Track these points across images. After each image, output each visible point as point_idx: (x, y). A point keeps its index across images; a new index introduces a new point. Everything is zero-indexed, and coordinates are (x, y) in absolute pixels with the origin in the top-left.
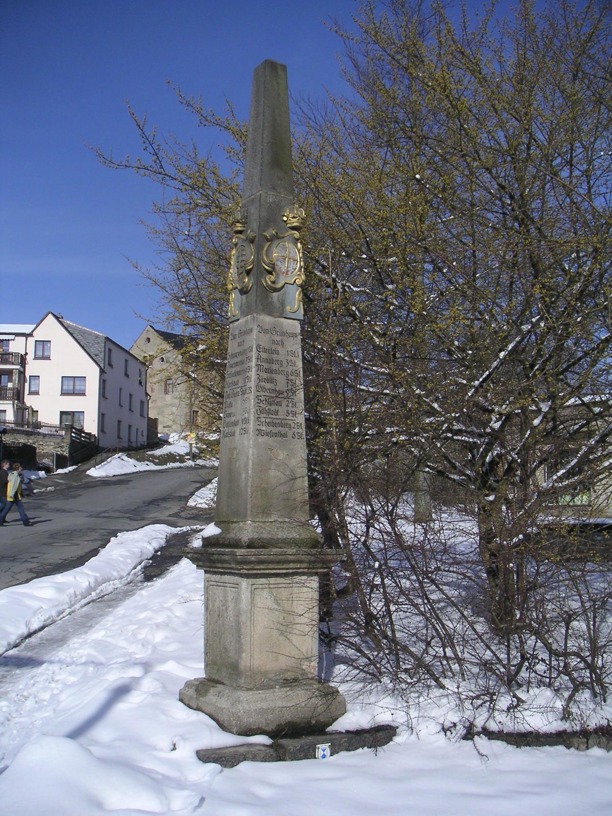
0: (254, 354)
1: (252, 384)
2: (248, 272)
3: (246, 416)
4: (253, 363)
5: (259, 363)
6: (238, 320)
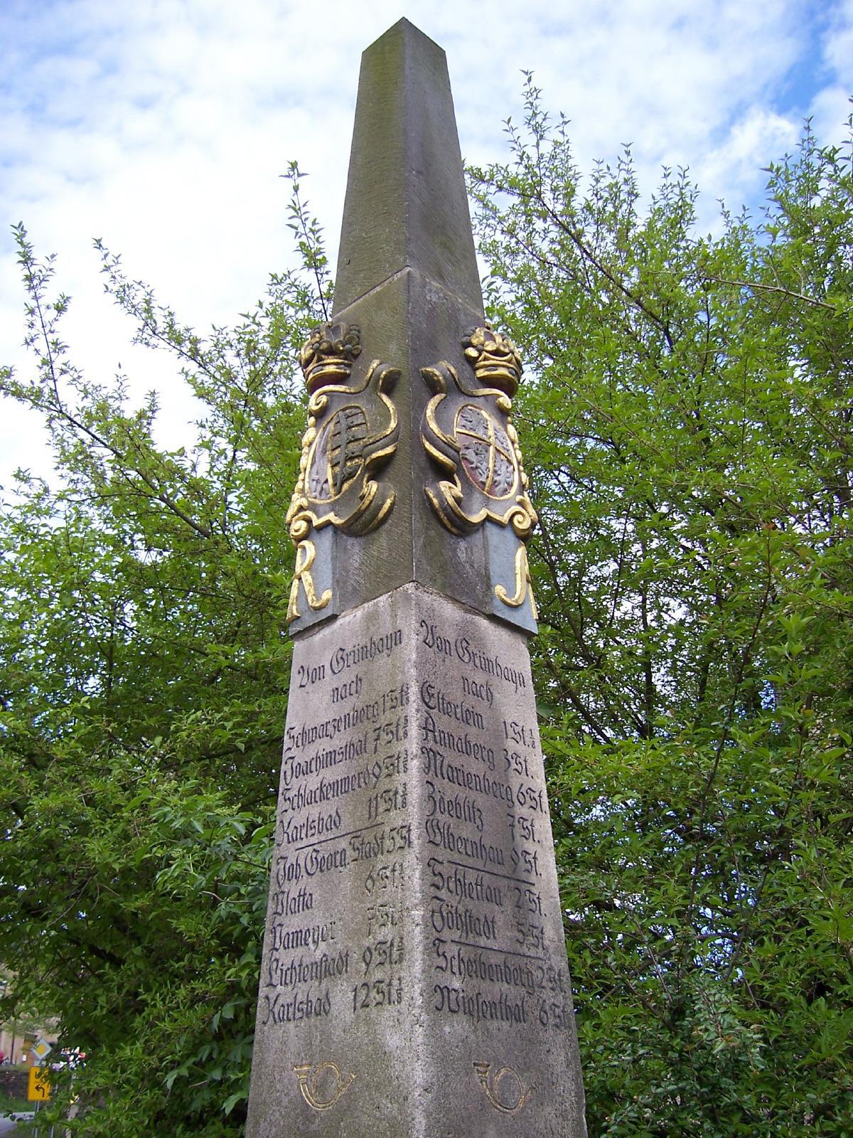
0: (413, 709)
1: (414, 814)
2: (378, 469)
3: (387, 933)
4: (413, 742)
5: (431, 744)
6: (333, 618)
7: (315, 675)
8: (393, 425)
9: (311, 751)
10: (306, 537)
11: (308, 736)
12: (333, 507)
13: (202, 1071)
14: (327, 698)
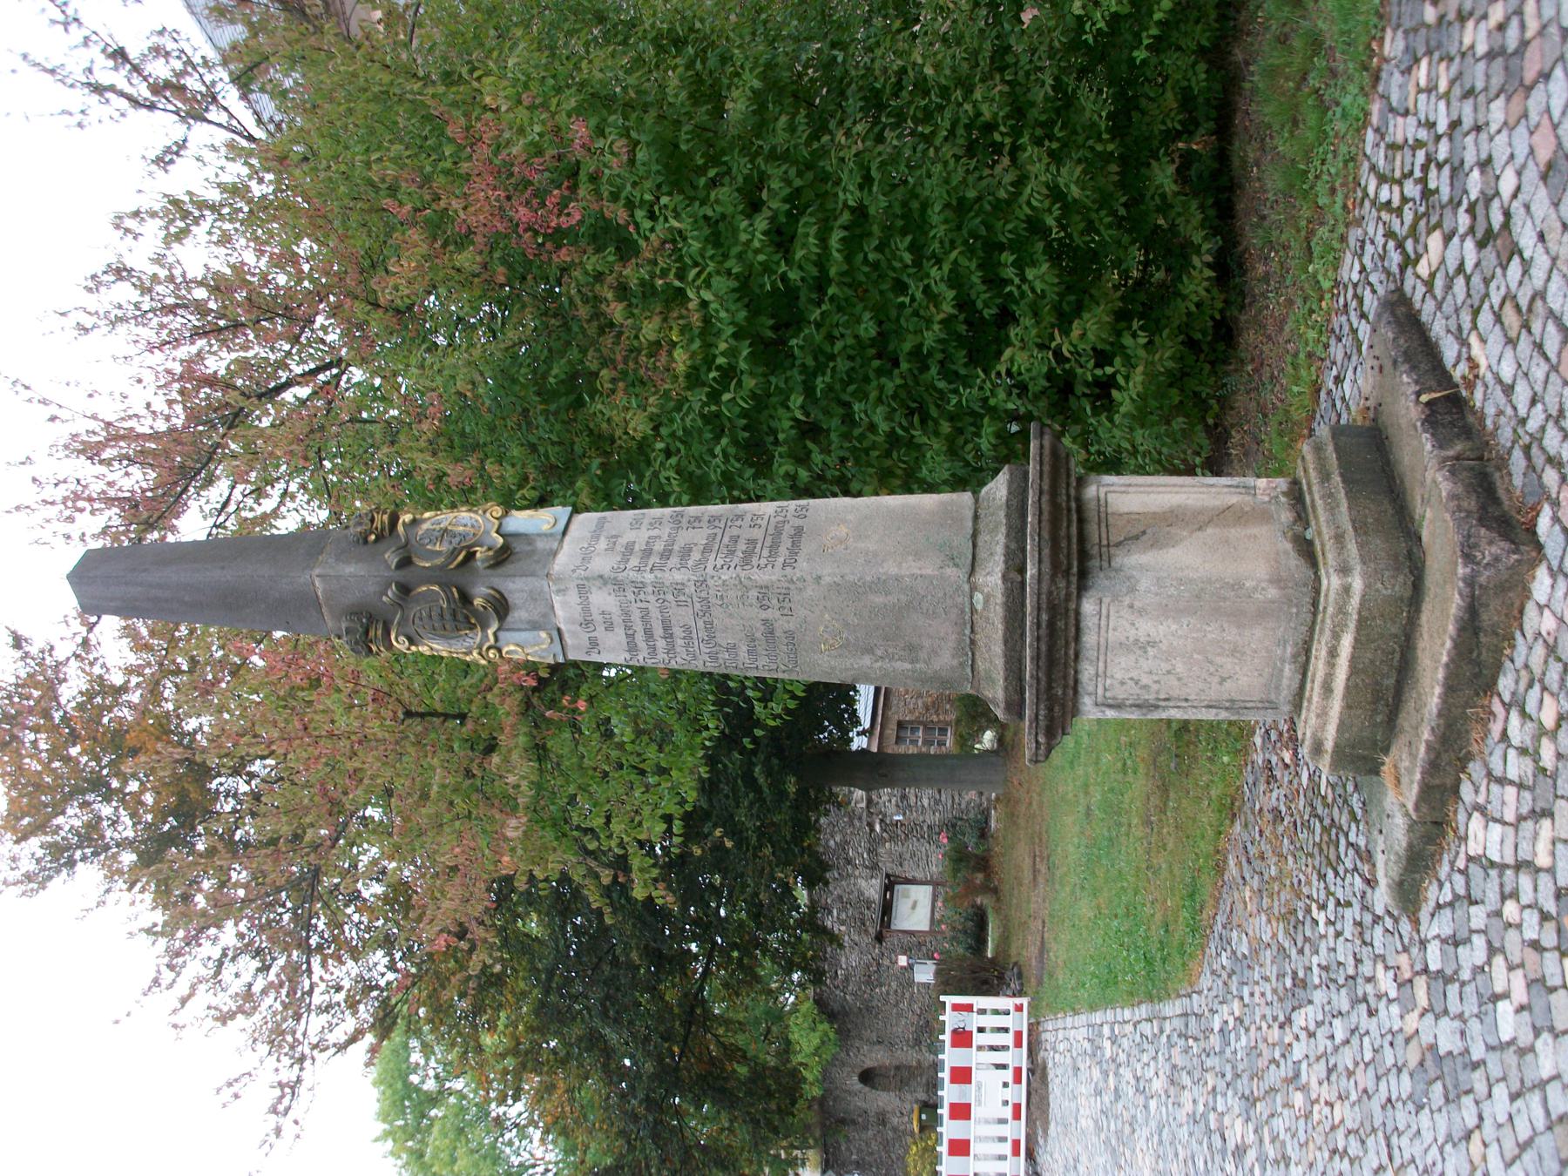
6: (559, 630)
7: (594, 643)
8: (436, 588)
9: (641, 644)
10: (500, 651)
11: (632, 648)
12: (484, 627)
13: (1268, 962)
14: (610, 634)
